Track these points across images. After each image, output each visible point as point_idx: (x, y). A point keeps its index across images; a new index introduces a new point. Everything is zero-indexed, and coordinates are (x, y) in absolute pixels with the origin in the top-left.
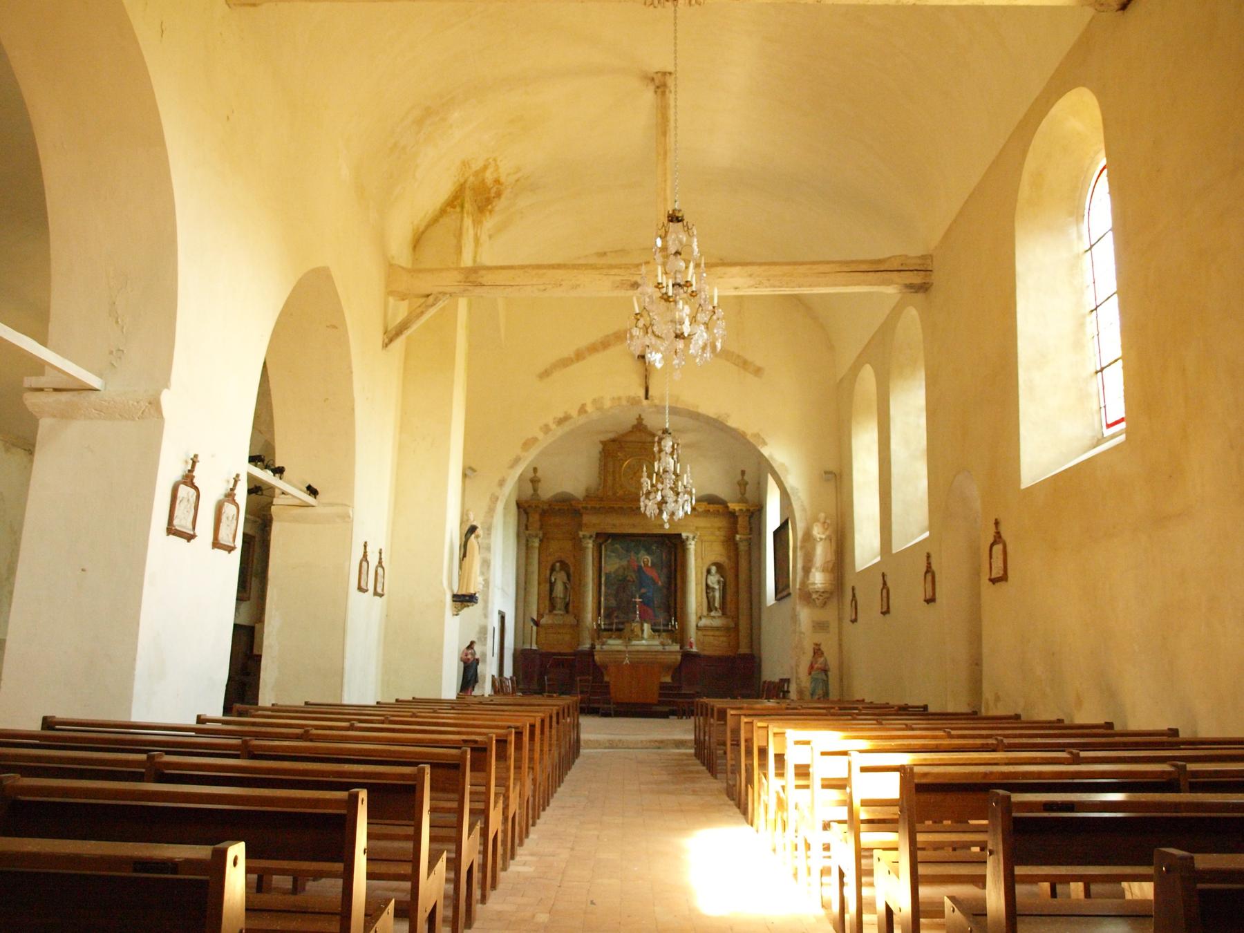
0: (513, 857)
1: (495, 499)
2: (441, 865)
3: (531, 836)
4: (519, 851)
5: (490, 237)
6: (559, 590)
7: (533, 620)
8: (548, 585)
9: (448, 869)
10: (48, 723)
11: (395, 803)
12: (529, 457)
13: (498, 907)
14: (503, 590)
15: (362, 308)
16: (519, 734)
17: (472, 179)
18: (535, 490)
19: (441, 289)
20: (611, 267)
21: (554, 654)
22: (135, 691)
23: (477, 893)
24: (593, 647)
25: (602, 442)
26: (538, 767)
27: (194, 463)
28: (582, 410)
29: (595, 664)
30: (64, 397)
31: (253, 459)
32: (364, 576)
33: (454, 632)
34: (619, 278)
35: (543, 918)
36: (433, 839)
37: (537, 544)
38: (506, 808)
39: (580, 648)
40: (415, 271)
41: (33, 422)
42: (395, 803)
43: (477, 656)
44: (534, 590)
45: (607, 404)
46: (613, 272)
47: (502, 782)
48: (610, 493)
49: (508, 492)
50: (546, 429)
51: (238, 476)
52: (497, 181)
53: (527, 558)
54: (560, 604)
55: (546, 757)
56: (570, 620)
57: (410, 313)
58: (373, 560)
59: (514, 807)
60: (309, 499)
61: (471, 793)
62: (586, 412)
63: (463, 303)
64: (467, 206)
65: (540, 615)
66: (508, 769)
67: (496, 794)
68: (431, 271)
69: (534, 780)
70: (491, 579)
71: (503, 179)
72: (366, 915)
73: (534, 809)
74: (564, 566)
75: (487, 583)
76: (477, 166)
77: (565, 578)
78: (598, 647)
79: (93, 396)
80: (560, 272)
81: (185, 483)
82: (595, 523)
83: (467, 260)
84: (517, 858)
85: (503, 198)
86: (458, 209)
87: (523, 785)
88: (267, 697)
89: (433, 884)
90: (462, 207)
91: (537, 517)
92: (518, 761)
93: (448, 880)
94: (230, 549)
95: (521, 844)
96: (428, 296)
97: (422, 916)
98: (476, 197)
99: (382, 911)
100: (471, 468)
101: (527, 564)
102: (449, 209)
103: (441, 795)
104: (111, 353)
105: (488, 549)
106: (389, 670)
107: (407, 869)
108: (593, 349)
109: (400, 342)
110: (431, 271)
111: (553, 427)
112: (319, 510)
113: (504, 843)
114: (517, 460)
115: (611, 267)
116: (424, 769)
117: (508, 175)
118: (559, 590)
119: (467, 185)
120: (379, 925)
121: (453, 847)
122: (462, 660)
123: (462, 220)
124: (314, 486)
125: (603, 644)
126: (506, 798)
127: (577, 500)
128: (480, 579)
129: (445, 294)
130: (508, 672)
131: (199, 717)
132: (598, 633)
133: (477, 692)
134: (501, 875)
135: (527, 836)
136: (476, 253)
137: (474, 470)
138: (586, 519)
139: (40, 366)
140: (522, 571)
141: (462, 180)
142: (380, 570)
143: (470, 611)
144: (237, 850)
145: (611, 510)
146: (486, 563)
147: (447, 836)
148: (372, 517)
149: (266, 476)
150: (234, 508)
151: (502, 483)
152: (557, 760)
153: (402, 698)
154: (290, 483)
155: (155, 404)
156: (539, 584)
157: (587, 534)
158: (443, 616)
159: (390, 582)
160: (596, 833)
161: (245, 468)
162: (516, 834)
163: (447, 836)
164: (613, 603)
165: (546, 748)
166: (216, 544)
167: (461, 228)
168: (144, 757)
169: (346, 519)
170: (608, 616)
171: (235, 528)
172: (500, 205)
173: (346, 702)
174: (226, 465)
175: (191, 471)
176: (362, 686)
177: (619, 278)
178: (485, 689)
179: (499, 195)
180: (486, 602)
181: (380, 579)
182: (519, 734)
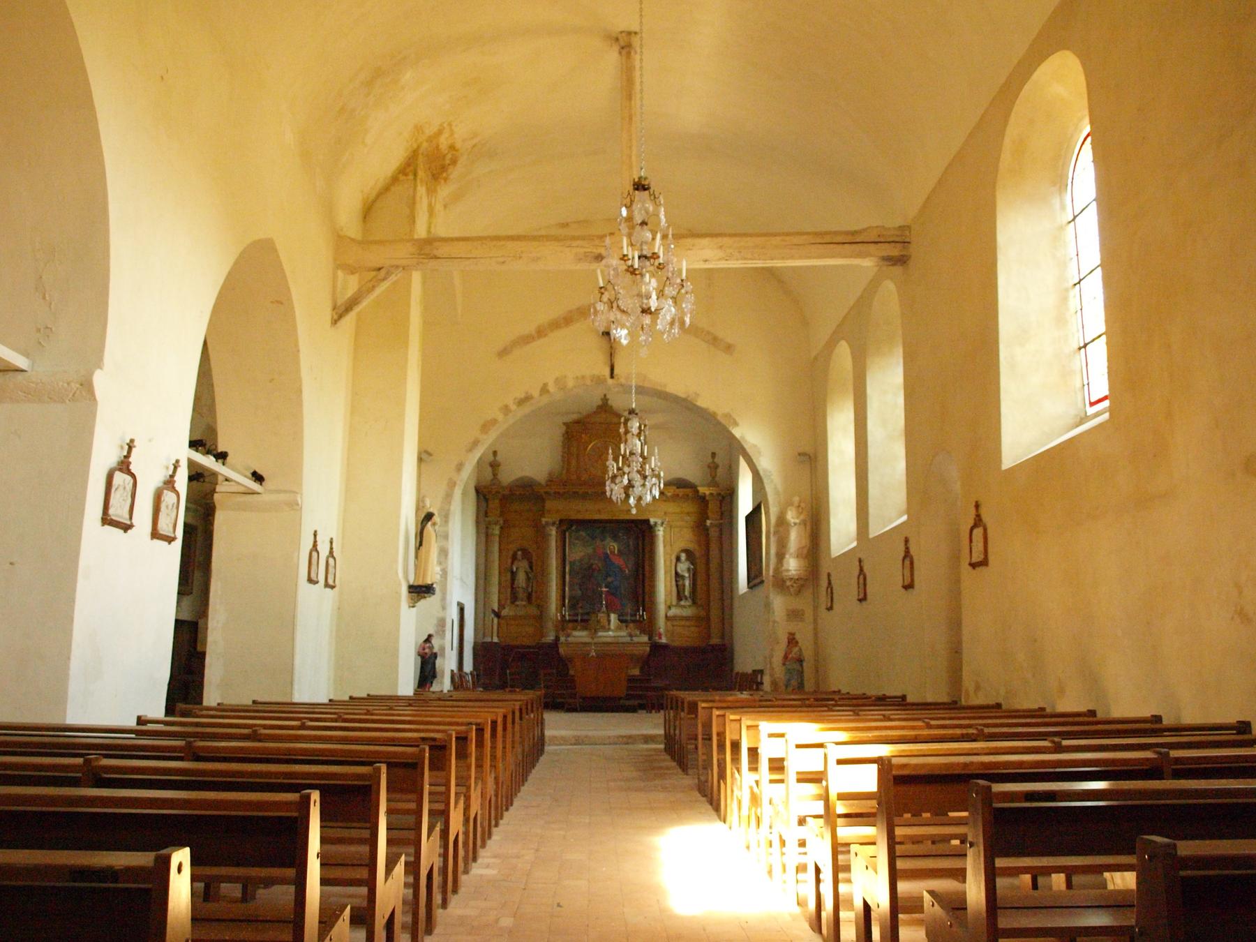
1: (452, 484)
2: (400, 868)
3: (494, 837)
4: (482, 853)
5: (445, 207)
6: (521, 578)
8: (509, 575)
9: (406, 873)
11: (351, 805)
14: (461, 579)
15: (310, 283)
16: (480, 731)
17: (425, 145)
18: (495, 475)
23: (438, 898)
24: (557, 639)
27: (130, 448)
28: (544, 390)
33: (411, 625)
34: (582, 250)
35: (506, 922)
36: (390, 842)
37: (497, 531)
39: (544, 640)
40: (365, 243)
42: (351, 805)
43: (436, 650)
44: (495, 580)
45: (571, 384)
47: (463, 782)
48: (574, 477)
49: (467, 475)
50: (506, 410)
51: (177, 461)
52: (452, 147)
55: (509, 754)
56: (533, 610)
58: (324, 550)
59: (475, 807)
60: (255, 486)
62: (548, 391)
63: (416, 277)
64: (421, 174)
65: (501, 606)
66: (469, 767)
68: (381, 242)
71: (458, 145)
74: (526, 554)
75: (444, 573)
76: (429, 131)
78: (562, 639)
79: (20, 376)
81: (121, 470)
82: (557, 509)
83: (421, 231)
84: (480, 861)
85: (459, 165)
86: (411, 177)
87: (484, 783)
88: (212, 696)
89: (391, 889)
90: (415, 175)
93: (406, 885)
94: (170, 540)
95: (483, 846)
98: (429, 164)
100: (426, 452)
101: (487, 552)
102: (401, 177)
103: (398, 796)
106: (342, 665)
107: (363, 873)
108: (555, 325)
110: (381, 242)
111: (513, 407)
112: (266, 497)
113: (466, 844)
114: (476, 443)
115: (574, 238)
118: (521, 578)
121: (412, 850)
124: (259, 471)
125: (568, 636)
126: (467, 798)
129: (397, 267)
130: (468, 667)
131: (139, 718)
132: (563, 625)
133: (435, 687)
134: (463, 878)
137: (430, 454)
138: (549, 504)
141: (415, 146)
142: (331, 560)
146: (444, 552)
147: (405, 838)
148: (322, 507)
149: (208, 462)
150: (174, 496)
151: (460, 467)
152: (520, 757)
153: (355, 695)
154: (233, 468)
155: (87, 386)
157: (550, 520)
158: (398, 608)
160: (562, 833)
161: (185, 453)
163: (405, 838)
166: (155, 534)
167: (414, 197)
169: (295, 506)
170: (573, 606)
171: (175, 517)
172: (455, 173)
174: (165, 449)
175: (127, 457)
176: (313, 684)
177: (582, 250)
178: (444, 684)
179: (454, 162)
181: (331, 570)
182: (480, 731)
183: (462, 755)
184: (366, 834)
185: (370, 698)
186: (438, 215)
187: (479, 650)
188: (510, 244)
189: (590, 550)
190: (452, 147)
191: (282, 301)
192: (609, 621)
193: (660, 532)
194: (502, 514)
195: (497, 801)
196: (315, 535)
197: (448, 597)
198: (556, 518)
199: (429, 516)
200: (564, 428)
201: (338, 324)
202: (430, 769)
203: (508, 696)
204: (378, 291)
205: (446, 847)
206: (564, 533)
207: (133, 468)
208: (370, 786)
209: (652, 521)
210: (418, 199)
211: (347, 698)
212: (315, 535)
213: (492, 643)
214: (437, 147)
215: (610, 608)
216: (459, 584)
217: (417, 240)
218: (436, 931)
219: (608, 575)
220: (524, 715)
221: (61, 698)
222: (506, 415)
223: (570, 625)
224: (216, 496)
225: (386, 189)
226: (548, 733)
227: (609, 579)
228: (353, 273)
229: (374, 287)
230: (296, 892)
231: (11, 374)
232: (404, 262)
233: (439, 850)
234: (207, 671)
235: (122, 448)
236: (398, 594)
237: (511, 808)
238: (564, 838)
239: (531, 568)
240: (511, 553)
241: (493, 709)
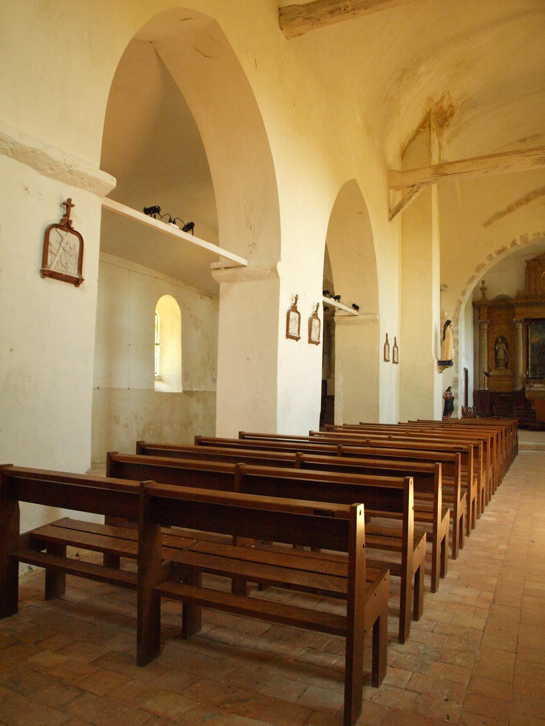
0: (482, 512)
1: (460, 303)
2: (448, 515)
3: (492, 500)
4: (486, 508)
5: (448, 142)
6: (501, 354)
7: (485, 373)
8: (494, 352)
9: (451, 517)
10: (242, 435)
11: (426, 483)
12: (480, 276)
13: (476, 539)
14: (466, 356)
15: (376, 200)
16: (485, 443)
17: (434, 107)
18: (484, 295)
19: (421, 181)
20: (531, 150)
21: (499, 393)
22: (278, 419)
23: (464, 531)
24: (524, 388)
25: (526, 261)
26: (495, 462)
27: (296, 299)
28: (514, 243)
29: (525, 399)
30: (230, 271)
31: (325, 293)
32: (387, 353)
33: (439, 382)
34: (537, 157)
35: (503, 547)
36: (443, 501)
37: (486, 327)
38: (479, 484)
39: (516, 389)
40: (403, 172)
41: (217, 286)
42: (426, 483)
43: (453, 395)
44: (485, 355)
45: (530, 238)
46: (532, 153)
47: (477, 470)
48: (533, 293)
49: (468, 297)
50: (490, 257)
51: (318, 304)
52: (451, 106)
53: (480, 336)
54: (501, 363)
55: (499, 456)
56: (509, 372)
57: (403, 199)
58: (391, 343)
59: (483, 484)
60: (354, 312)
61: (462, 476)
62: (516, 244)
63: (434, 187)
64: (433, 126)
65: (489, 370)
66: (480, 464)
67: (474, 477)
68: (414, 170)
69: (493, 469)
70: (460, 350)
71: (454, 104)
72: (414, 540)
73: (493, 486)
74: (504, 340)
75: (457, 352)
76: (437, 99)
77: (505, 348)
78: (527, 389)
79: (244, 269)
80: (496, 159)
81: (293, 311)
82: (522, 312)
83: (435, 161)
84: (485, 512)
85: (455, 116)
86: (427, 129)
87: (487, 472)
88: (339, 421)
89: (444, 525)
90: (430, 127)
91: (486, 310)
92: (485, 457)
93: (451, 523)
94: (317, 343)
95: (487, 505)
96: (413, 186)
97: (439, 542)
98: (438, 118)
99: (421, 538)
100: (444, 285)
101: (480, 340)
102: (422, 130)
103: (447, 477)
104: (250, 245)
105: (457, 332)
106: (403, 404)
107: (430, 516)
108: (519, 203)
109: (398, 216)
110: (414, 170)
111: (495, 256)
112: (360, 317)
113: (478, 503)
114: (473, 278)
115: (531, 150)
116: (438, 465)
117: (458, 100)
118: (501, 354)
119: (432, 112)
120: (420, 545)
121: (452, 505)
122: (444, 397)
123: (430, 135)
124: (357, 304)
125: (531, 387)
126: (479, 480)
127: (511, 299)
128: (453, 350)
129: (424, 183)
130: (471, 404)
131: (310, 432)
132: (527, 380)
133: (453, 416)
134: (477, 521)
135: (490, 500)
136: (440, 154)
137: (446, 287)
138: (518, 310)
139: (216, 257)
140: (477, 344)
141: (428, 110)
142: (395, 349)
143: (449, 370)
144: (361, 508)
145: (534, 304)
146: (456, 341)
147: (450, 499)
148: (389, 320)
149: (331, 301)
150: (317, 321)
151: (463, 293)
152: (505, 457)
153: (411, 420)
154: (343, 304)
155: (275, 270)
156: (488, 351)
157: (519, 320)
158: (433, 373)
159: (401, 357)
160: (532, 501)
161: (321, 299)
162: (484, 499)
163: (450, 499)
164: (537, 362)
165: (499, 450)
166: (310, 341)
167: (430, 140)
168: (294, 455)
169: (375, 321)
170: (534, 369)
171: (319, 333)
172: (453, 121)
173: (381, 422)
174: (312, 299)
175: (295, 304)
176: (389, 414)
177: (537, 157)
178: (458, 414)
179: (452, 114)
180: (457, 364)
181: (396, 354)
182: (485, 443)
183: (476, 456)
184: (432, 496)
185: (419, 422)
186: (446, 148)
187: (477, 394)
188: (490, 160)
190: (451, 106)
191: (362, 212)
194: (489, 317)
195: (493, 480)
196: (387, 336)
197: (459, 366)
198: (523, 317)
199: (448, 323)
200: (526, 264)
201: (392, 220)
202: (461, 464)
203: (495, 422)
204: (413, 198)
205: (468, 503)
206: (527, 326)
207: (298, 309)
208: (434, 474)
210: (432, 141)
211: (407, 422)
212: (387, 336)
213: (484, 390)
214: (442, 107)
216: (465, 360)
217: (433, 166)
218: (464, 547)
220: (507, 433)
221: (274, 422)
222: (490, 260)
223: (532, 380)
224: (335, 318)
225: (414, 138)
226: (520, 443)
228: (398, 190)
229: (411, 196)
230: (404, 523)
231: (240, 268)
232: (427, 180)
233: (466, 506)
234: (335, 407)
235: (292, 299)
236: (433, 366)
237: (501, 485)
238: (533, 503)
239: (507, 348)
240: (495, 339)
241: (490, 431)
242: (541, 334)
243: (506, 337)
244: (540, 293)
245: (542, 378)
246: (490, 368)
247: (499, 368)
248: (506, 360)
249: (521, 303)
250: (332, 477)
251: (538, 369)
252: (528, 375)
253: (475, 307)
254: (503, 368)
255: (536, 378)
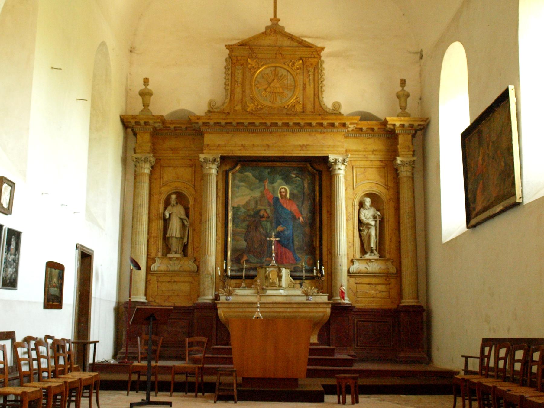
8: (161, 223)
24: (217, 297)
25: (228, 47)
54: (175, 245)
56: (189, 265)
74: (181, 198)
77: (184, 216)
78: (223, 298)
82: (218, 144)
91: (147, 137)
101: (135, 196)
125: (230, 294)
131: (171, 406)
138: (208, 139)
156: (150, 221)
157: (211, 157)
164: (243, 244)
170: (237, 260)
189: (257, 194)
192: (280, 277)
193: (341, 172)
206: (226, 174)
209: (331, 158)
215: (281, 262)
219: (278, 223)
223: (233, 282)
227: (280, 228)
239: (187, 215)
240: (164, 197)
242: (252, 190)
243: (186, 192)
244: (251, 107)
245: (252, 277)
246: (153, 255)
247: (169, 256)
248: (186, 240)
249: (215, 124)
250: (495, 353)
251: (245, 258)
252: (226, 271)
253: (129, 130)
254: (178, 256)
255: (240, 277)
